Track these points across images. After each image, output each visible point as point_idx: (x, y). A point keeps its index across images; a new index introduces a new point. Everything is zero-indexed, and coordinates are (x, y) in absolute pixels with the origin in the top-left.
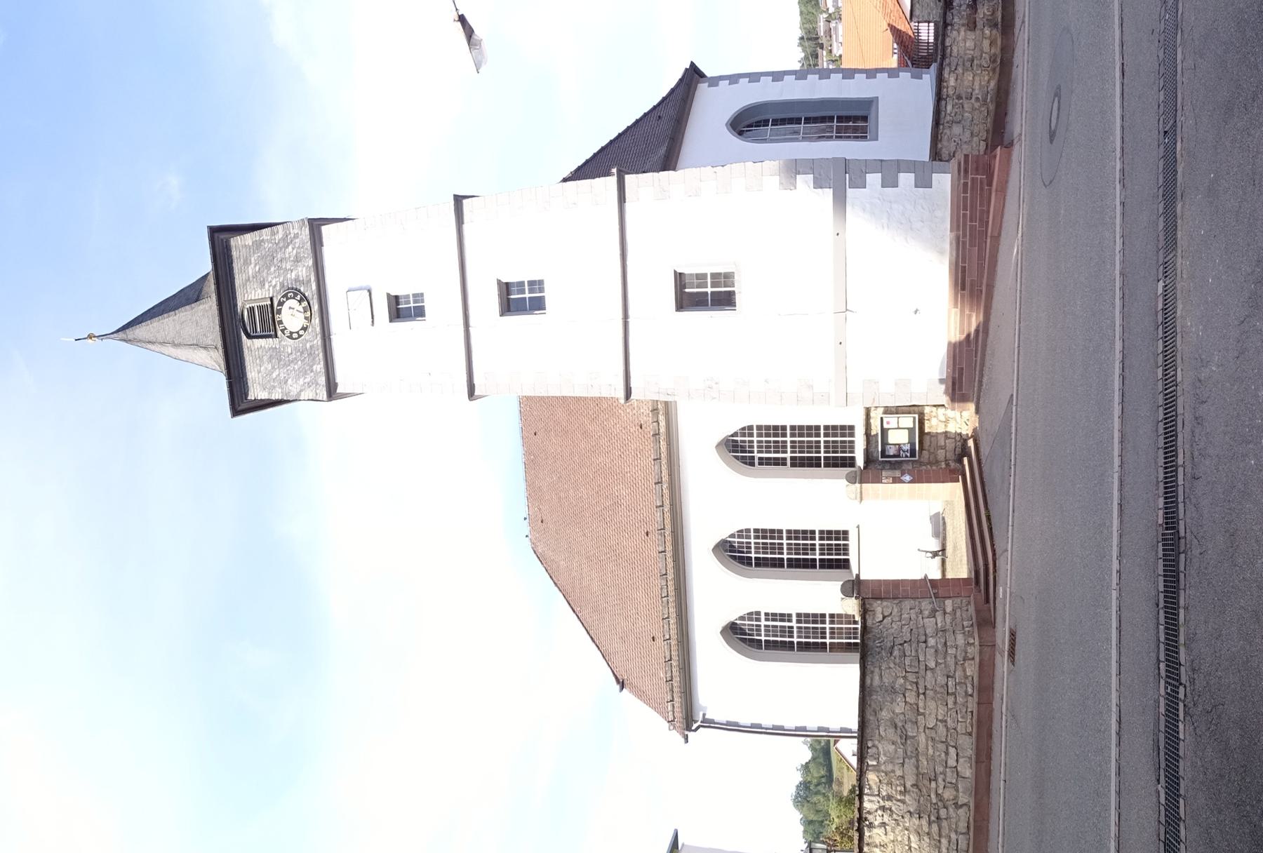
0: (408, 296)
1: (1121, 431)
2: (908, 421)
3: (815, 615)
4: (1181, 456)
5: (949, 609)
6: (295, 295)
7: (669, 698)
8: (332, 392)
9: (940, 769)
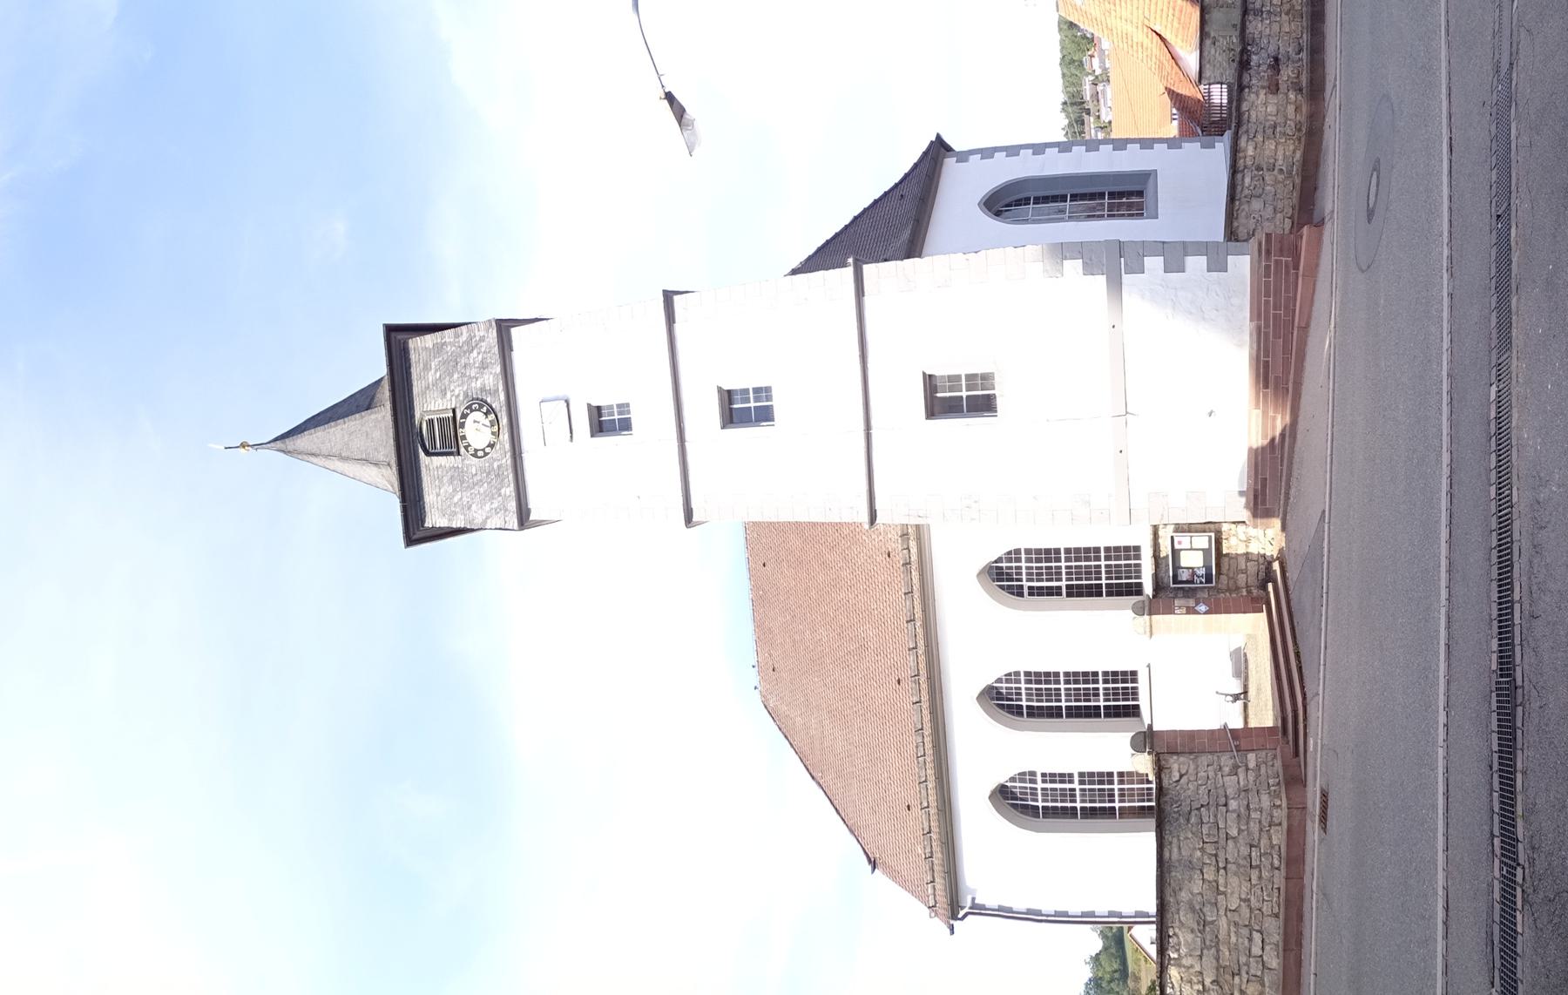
0: (611, 407)
1: (1449, 558)
2: (1202, 541)
3: (1101, 774)
4: (1517, 590)
5: (1252, 765)
6: (481, 406)
7: (929, 878)
8: (524, 519)
9: (1243, 959)
